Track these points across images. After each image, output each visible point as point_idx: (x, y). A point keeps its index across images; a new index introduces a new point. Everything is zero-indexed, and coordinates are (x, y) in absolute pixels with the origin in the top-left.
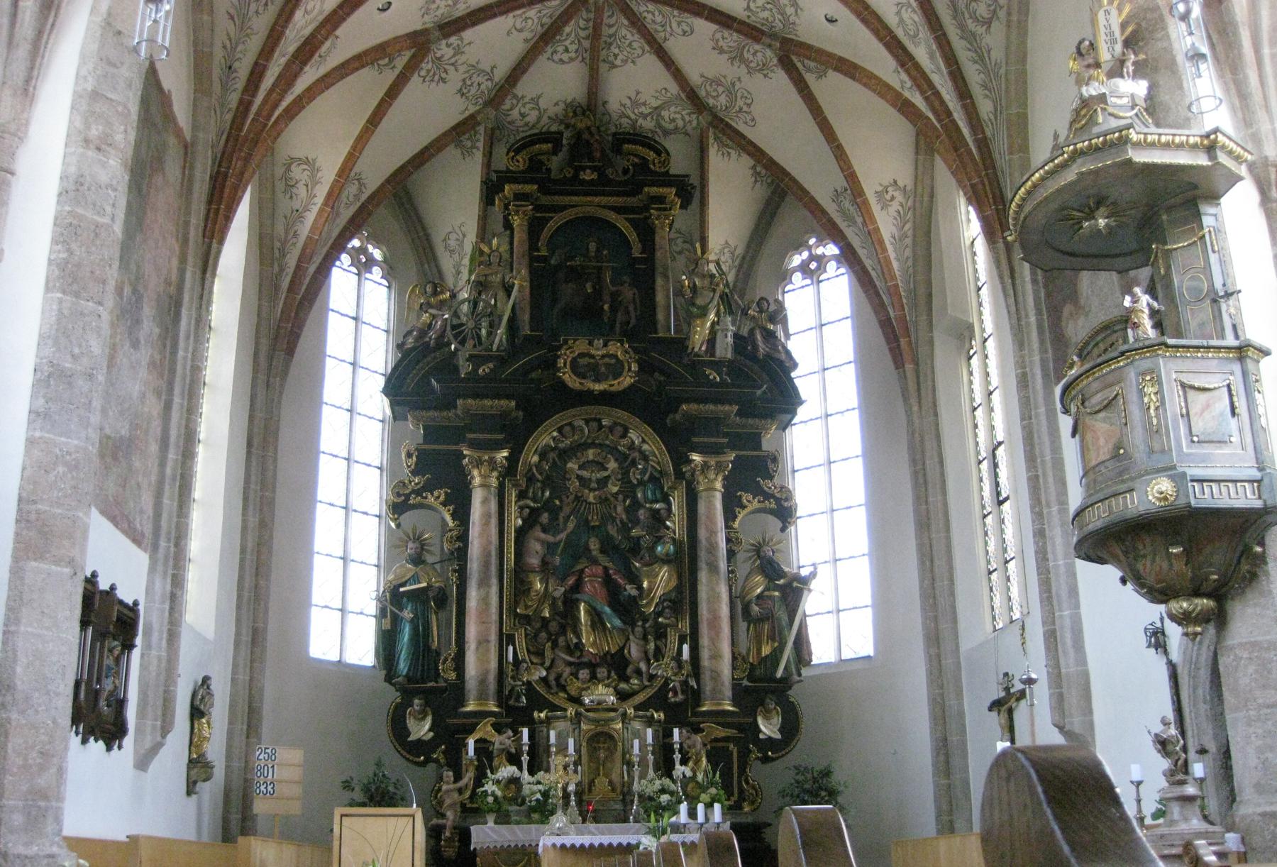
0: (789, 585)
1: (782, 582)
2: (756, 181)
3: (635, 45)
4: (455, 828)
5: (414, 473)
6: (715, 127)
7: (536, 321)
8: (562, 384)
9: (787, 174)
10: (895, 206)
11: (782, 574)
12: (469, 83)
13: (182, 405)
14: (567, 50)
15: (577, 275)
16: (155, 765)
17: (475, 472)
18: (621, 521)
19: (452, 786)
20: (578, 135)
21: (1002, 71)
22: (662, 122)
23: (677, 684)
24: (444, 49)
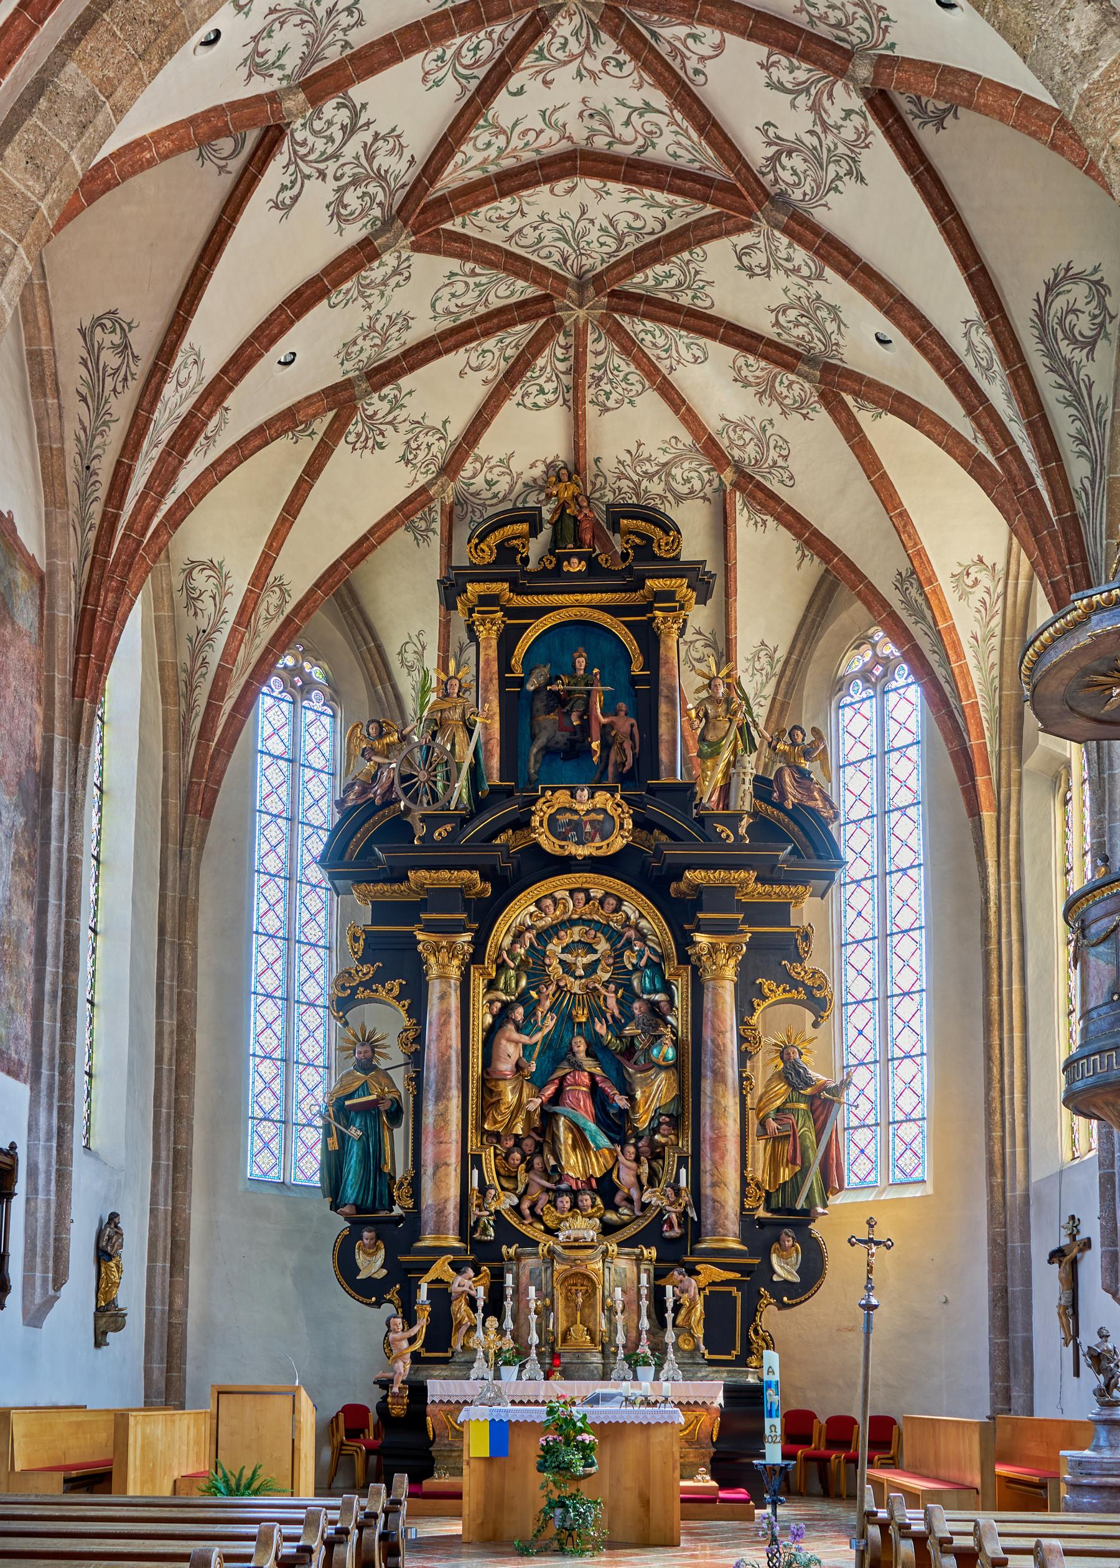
2: (804, 556)
3: (633, 378)
5: (362, 961)
7: (509, 765)
8: (537, 846)
9: (837, 551)
10: (979, 592)
11: (808, 1082)
12: (414, 445)
13: (59, 907)
14: (542, 391)
16: (52, 1317)
17: (432, 960)
18: (613, 1016)
21: (1108, 415)
22: (674, 484)
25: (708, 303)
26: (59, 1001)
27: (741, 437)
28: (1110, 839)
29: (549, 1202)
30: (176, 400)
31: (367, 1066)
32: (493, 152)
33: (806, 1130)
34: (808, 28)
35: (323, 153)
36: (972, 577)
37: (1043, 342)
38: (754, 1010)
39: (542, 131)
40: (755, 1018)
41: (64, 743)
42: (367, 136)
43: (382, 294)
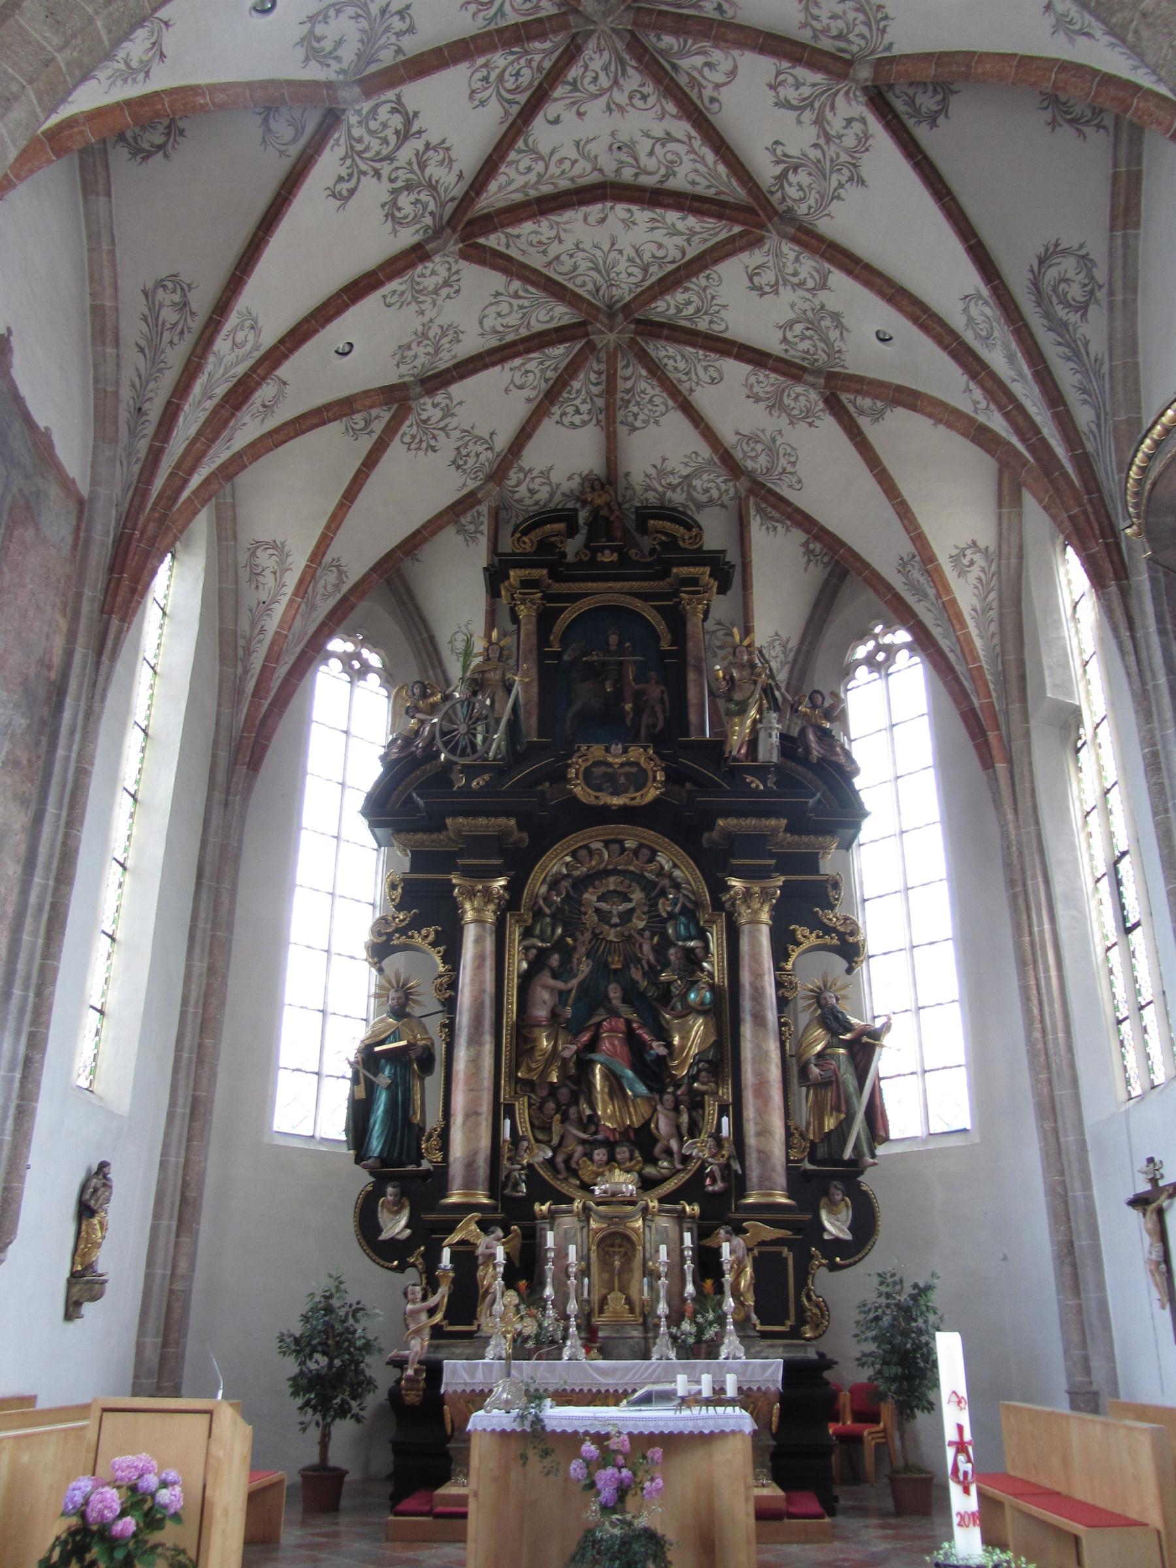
0: (856, 1041)
1: (848, 1036)
2: (809, 561)
3: (657, 400)
4: (420, 1362)
6: (756, 495)
7: (545, 726)
8: (574, 798)
9: (842, 544)
10: (975, 572)
11: (848, 1027)
13: (59, 817)
14: (578, 412)
15: (595, 672)
17: (468, 906)
19: (419, 1305)
20: (595, 512)
21: (1105, 369)
23: (715, 1168)
24: (429, 408)
25: (722, 327)
26: (45, 916)
27: (753, 449)
28: (1164, 747)
29: (585, 1155)
30: (230, 357)
31: (400, 1012)
32: (532, 177)
33: (848, 1077)
34: (812, 43)
35: (378, 153)
36: (968, 558)
37: (1039, 306)
38: (788, 956)
39: (576, 161)
40: (790, 963)
41: (85, 656)
42: (419, 144)
43: (434, 303)
